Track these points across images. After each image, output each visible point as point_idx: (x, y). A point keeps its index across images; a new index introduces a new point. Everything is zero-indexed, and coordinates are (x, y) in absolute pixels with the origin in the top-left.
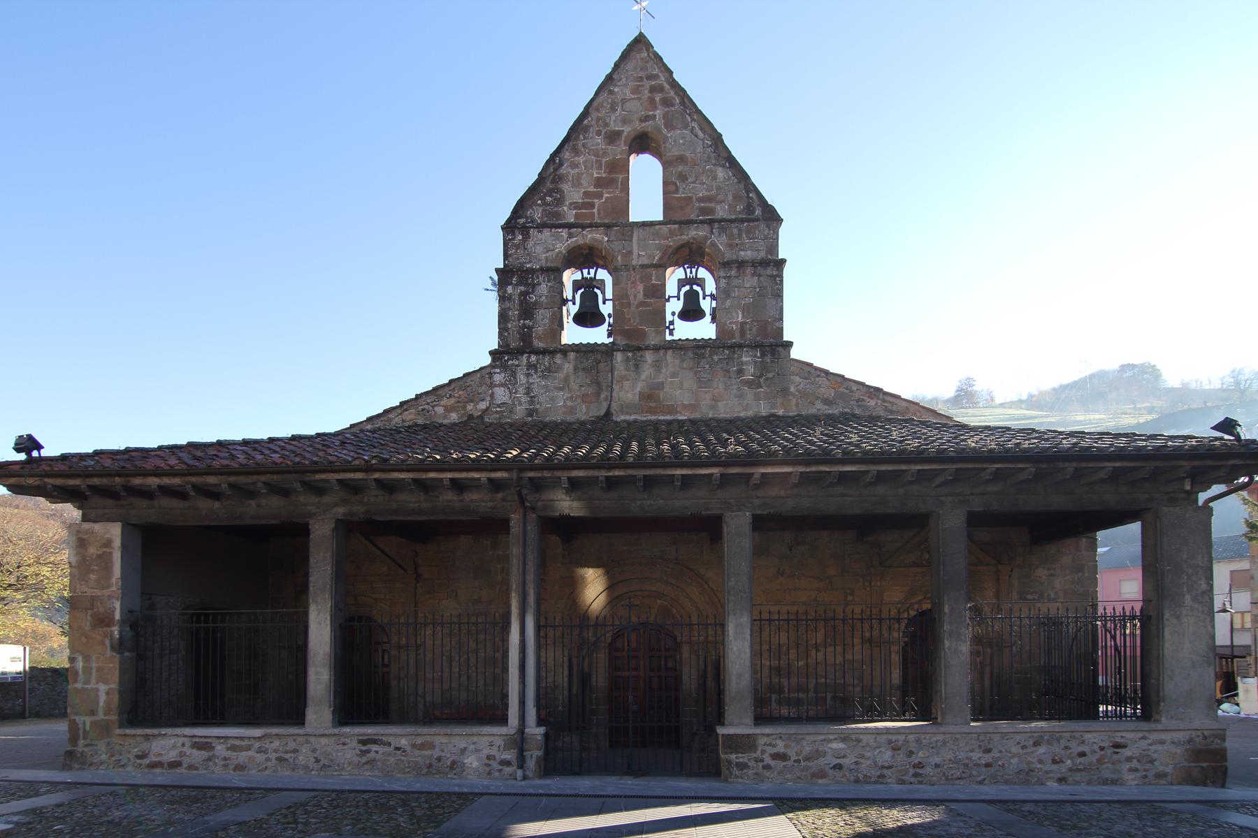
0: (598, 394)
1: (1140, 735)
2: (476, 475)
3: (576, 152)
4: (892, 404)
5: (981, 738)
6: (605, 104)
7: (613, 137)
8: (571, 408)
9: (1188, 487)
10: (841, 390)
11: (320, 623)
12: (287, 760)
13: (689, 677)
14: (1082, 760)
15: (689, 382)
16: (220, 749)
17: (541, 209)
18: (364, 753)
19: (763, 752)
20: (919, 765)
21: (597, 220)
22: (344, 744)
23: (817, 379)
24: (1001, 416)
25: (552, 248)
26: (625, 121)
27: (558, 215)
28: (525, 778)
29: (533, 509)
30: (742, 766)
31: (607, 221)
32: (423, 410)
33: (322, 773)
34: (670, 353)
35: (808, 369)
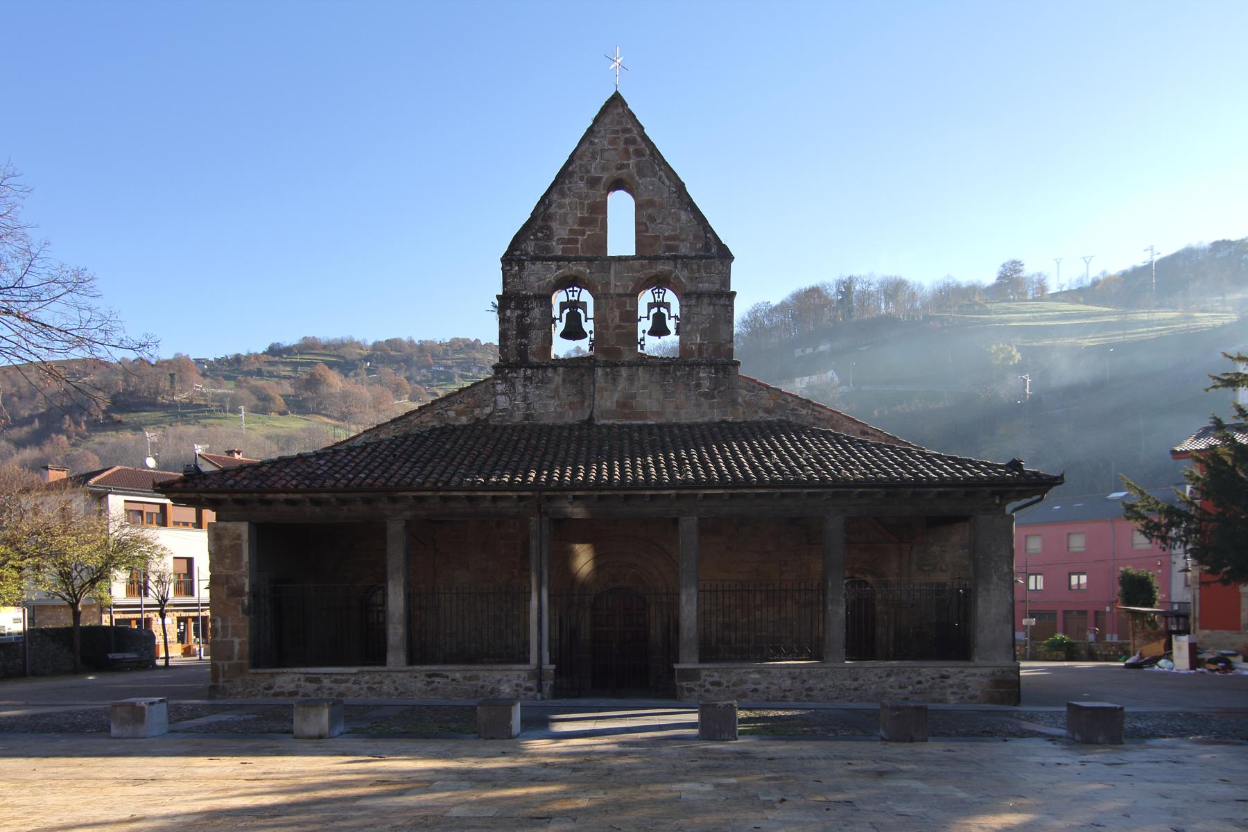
0: (582, 402)
1: (959, 670)
2: (510, 494)
3: (563, 195)
4: (820, 413)
5: (852, 671)
6: (587, 153)
9: (997, 502)
10: (779, 401)
11: (396, 593)
12: (374, 689)
14: (919, 686)
16: (326, 682)
17: (533, 243)
18: (429, 683)
19: (705, 680)
20: (810, 689)
21: (580, 254)
22: (415, 677)
23: (760, 392)
25: (543, 278)
26: (604, 168)
27: (548, 249)
28: (542, 699)
30: (691, 690)
31: (589, 255)
32: (438, 413)
33: (400, 698)
34: (641, 369)
35: (752, 384)
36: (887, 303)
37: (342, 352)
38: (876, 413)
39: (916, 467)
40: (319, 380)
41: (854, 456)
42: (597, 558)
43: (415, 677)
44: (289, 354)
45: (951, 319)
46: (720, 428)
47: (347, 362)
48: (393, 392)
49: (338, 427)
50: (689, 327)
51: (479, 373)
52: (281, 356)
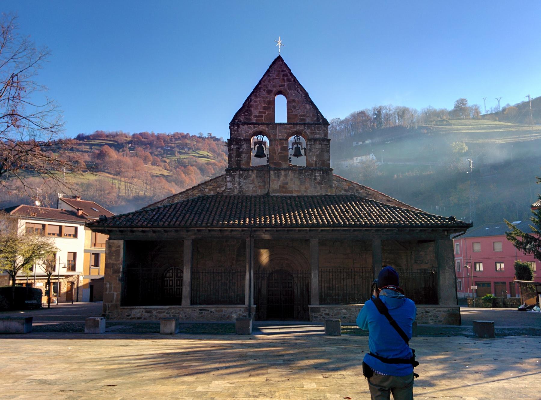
0: (264, 186)
1: (433, 309)
2: (238, 229)
3: (256, 97)
4: (369, 192)
7: (269, 92)
8: (255, 190)
9: (446, 234)
13: (297, 291)
15: (297, 182)
16: (154, 313)
19: (322, 313)
21: (264, 122)
22: (194, 311)
24: (482, 126)
26: (274, 86)
27: (250, 119)
29: (253, 237)
30: (316, 317)
31: (267, 122)
35: (338, 178)
36: (399, 119)
37: (116, 138)
38: (396, 176)
39: (411, 218)
40: (105, 154)
41: (384, 213)
42: (270, 256)
43: (194, 311)
44: (88, 140)
45: (432, 128)
46: (325, 198)
47: (118, 144)
48: (143, 160)
49: (113, 179)
50: (311, 154)
51: (189, 151)
52: (84, 140)
